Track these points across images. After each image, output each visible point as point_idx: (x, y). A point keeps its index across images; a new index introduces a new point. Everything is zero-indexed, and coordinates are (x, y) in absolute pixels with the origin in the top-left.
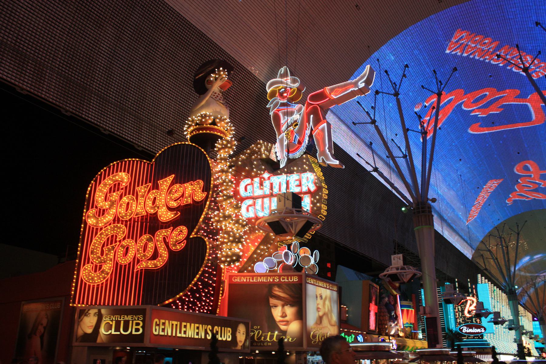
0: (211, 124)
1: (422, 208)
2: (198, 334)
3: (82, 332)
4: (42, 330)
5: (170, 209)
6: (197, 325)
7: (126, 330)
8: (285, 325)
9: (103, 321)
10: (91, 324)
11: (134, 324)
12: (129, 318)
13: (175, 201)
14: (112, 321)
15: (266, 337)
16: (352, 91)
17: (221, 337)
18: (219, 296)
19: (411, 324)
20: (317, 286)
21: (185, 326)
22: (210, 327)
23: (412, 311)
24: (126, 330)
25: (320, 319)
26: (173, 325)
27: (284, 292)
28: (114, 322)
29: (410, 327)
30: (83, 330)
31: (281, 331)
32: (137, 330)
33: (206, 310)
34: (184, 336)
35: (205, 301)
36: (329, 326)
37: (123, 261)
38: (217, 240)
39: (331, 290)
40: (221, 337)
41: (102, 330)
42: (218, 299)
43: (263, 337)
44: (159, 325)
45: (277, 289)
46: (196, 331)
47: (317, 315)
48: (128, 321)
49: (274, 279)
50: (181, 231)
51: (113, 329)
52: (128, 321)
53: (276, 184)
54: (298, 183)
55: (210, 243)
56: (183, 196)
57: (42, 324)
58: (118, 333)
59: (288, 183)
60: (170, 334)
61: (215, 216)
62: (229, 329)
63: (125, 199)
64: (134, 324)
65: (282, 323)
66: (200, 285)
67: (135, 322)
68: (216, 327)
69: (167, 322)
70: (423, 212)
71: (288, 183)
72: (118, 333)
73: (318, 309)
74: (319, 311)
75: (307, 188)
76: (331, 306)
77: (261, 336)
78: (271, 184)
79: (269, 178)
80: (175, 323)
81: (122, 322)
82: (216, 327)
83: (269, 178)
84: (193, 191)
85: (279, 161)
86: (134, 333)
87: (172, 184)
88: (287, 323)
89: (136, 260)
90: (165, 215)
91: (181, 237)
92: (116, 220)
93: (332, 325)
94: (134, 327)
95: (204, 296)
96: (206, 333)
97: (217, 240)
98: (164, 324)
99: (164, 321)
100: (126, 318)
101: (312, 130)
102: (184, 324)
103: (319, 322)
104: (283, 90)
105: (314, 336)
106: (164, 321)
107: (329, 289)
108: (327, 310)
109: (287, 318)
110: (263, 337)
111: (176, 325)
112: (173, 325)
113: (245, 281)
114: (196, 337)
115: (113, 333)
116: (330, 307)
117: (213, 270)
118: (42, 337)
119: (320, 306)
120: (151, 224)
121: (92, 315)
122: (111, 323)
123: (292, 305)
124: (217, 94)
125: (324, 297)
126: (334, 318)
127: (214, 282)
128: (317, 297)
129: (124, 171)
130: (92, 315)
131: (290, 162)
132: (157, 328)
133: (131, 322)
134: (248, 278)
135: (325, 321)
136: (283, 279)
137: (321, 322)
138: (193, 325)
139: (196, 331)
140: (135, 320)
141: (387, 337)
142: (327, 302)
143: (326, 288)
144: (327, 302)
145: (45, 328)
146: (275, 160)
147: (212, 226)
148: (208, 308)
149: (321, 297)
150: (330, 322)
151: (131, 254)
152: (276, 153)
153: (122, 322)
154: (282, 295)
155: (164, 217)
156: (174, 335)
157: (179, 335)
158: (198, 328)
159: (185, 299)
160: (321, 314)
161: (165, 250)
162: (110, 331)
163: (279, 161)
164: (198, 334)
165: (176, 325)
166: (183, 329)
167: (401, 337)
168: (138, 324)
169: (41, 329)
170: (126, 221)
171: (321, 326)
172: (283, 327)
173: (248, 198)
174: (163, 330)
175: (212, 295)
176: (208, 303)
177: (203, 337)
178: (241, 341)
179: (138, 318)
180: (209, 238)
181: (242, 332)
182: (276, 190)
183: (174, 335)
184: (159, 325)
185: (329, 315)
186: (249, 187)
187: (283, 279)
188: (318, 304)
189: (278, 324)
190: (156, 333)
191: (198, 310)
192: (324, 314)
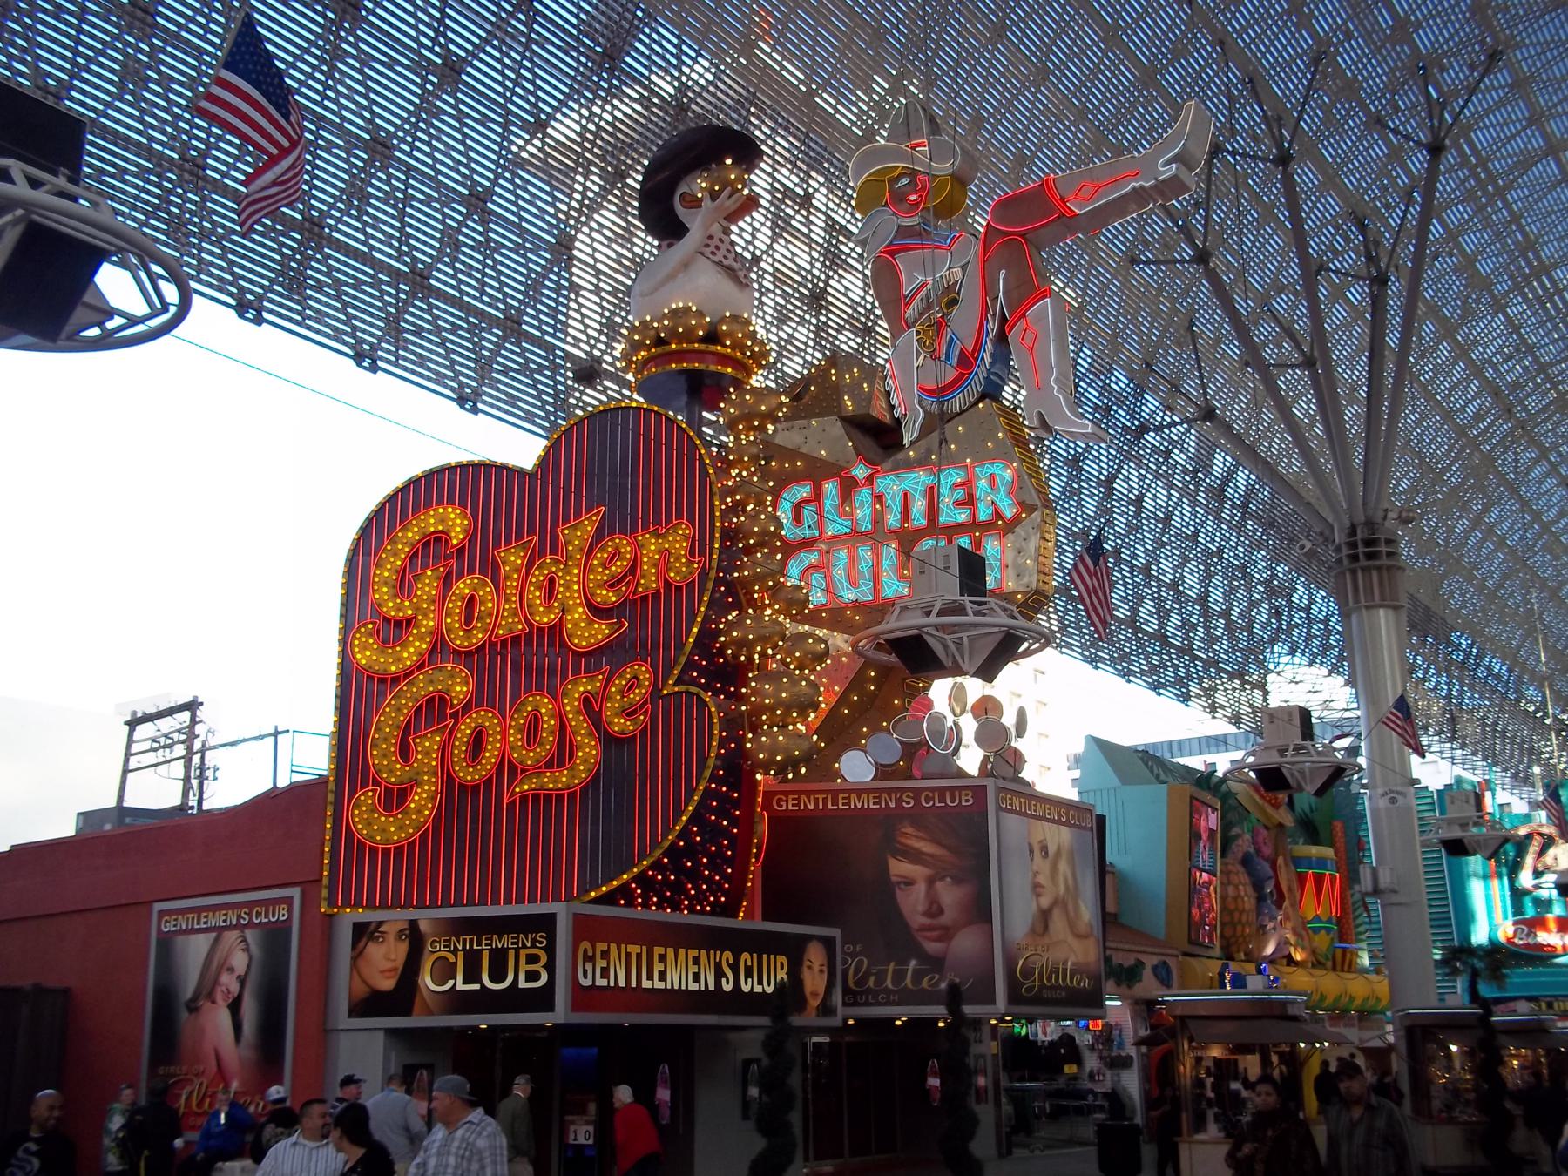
0: (703, 340)
1: (1368, 543)
2: (696, 978)
3: (366, 989)
4: (235, 988)
5: (598, 611)
6: (693, 952)
7: (497, 976)
8: (939, 939)
9: (426, 953)
10: (389, 965)
11: (523, 960)
12: (507, 941)
13: (612, 586)
14: (455, 952)
15: (880, 979)
16: (1134, 189)
17: (760, 982)
18: (748, 863)
19: (1329, 921)
20: (1031, 816)
21: (663, 958)
22: (728, 954)
23: (1333, 877)
24: (497, 976)
25: (1045, 916)
26: (628, 955)
27: (934, 841)
28: (461, 955)
29: (1328, 930)
30: (366, 983)
31: (924, 957)
32: (532, 976)
33: (710, 904)
34: (660, 985)
35: (709, 880)
36: (1071, 940)
37: (467, 775)
38: (741, 699)
39: (1073, 826)
40: (760, 982)
41: (427, 981)
42: (747, 871)
43: (872, 979)
44: (592, 959)
45: (909, 830)
46: (693, 969)
47: (1034, 907)
48: (504, 951)
49: (899, 801)
50: (636, 677)
51: (460, 978)
52: (504, 951)
53: (893, 498)
54: (960, 494)
55: (718, 707)
56: (633, 568)
57: (231, 970)
58: (477, 987)
59: (932, 494)
60: (622, 984)
61: (731, 626)
62: (782, 959)
63: (463, 587)
64: (523, 960)
65: (928, 934)
66: (697, 834)
67: (523, 952)
68: (745, 956)
69: (613, 947)
70: (1370, 556)
71: (932, 494)
72: (477, 987)
73: (1036, 888)
74: (1038, 895)
75: (990, 510)
76: (1074, 875)
77: (867, 974)
78: (879, 498)
79: (870, 480)
80: (634, 949)
81: (486, 954)
82: (745, 956)
83: (870, 480)
84: (665, 553)
85: (898, 421)
86: (522, 984)
87: (599, 536)
88: (946, 934)
89: (509, 769)
90: (587, 633)
91: (636, 696)
92: (439, 647)
93: (1079, 936)
94: (524, 967)
95: (706, 866)
96: (719, 974)
97: (741, 699)
98: (605, 955)
99: (604, 946)
100: (1330, 984)
101: (1003, 318)
102: (658, 950)
103: (1040, 929)
104: (905, 181)
105: (1028, 972)
106: (604, 946)
107: (1067, 824)
108: (1062, 889)
109: (946, 919)
110: (872, 979)
111: (639, 956)
112: (628, 955)
113: (811, 807)
114: (693, 987)
115: (460, 986)
116: (1070, 882)
117: (731, 789)
118: (235, 1007)
119: (1042, 879)
120: (532, 657)
121: (391, 938)
122: (452, 959)
123: (958, 881)
124: (716, 242)
125: (1052, 850)
126: (1087, 912)
127: (734, 822)
128: (1031, 852)
129: (451, 502)
130: (391, 938)
131: (937, 422)
132: (589, 966)
133: (511, 953)
134: (821, 797)
135: (1058, 923)
136: (928, 800)
137: (1046, 928)
138: (682, 951)
139: (693, 969)
140: (524, 946)
141: (1251, 967)
142: (1063, 866)
143: (1059, 822)
144: (1063, 866)
145: (242, 981)
146: (887, 419)
147: (723, 655)
148: (717, 899)
149: (1044, 849)
150: (1072, 925)
151: (490, 755)
152: (888, 393)
153: (486, 954)
154: (926, 847)
155: (581, 637)
156: (634, 985)
157: (646, 984)
158: (696, 961)
159: (654, 876)
160: (1045, 902)
161: (590, 735)
162: (451, 983)
163: (898, 421)
164: (696, 978)
165: (639, 956)
166: (658, 967)
167: (1296, 963)
168: (533, 959)
169: (229, 982)
170: (469, 654)
171: (1046, 940)
172: (932, 947)
173: (806, 544)
174: (605, 973)
175: (730, 862)
176: (719, 884)
177: (712, 987)
178: (815, 994)
179: (534, 941)
180: (716, 693)
181: (816, 968)
182: (893, 520)
183: (634, 985)
184: (592, 959)
185: (1070, 907)
186: (808, 513)
187: (928, 800)
188: (1036, 874)
189: (919, 937)
190: (587, 983)
191: (686, 907)
192: (1055, 903)
